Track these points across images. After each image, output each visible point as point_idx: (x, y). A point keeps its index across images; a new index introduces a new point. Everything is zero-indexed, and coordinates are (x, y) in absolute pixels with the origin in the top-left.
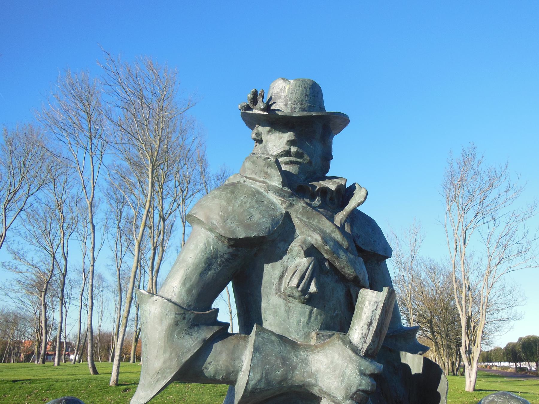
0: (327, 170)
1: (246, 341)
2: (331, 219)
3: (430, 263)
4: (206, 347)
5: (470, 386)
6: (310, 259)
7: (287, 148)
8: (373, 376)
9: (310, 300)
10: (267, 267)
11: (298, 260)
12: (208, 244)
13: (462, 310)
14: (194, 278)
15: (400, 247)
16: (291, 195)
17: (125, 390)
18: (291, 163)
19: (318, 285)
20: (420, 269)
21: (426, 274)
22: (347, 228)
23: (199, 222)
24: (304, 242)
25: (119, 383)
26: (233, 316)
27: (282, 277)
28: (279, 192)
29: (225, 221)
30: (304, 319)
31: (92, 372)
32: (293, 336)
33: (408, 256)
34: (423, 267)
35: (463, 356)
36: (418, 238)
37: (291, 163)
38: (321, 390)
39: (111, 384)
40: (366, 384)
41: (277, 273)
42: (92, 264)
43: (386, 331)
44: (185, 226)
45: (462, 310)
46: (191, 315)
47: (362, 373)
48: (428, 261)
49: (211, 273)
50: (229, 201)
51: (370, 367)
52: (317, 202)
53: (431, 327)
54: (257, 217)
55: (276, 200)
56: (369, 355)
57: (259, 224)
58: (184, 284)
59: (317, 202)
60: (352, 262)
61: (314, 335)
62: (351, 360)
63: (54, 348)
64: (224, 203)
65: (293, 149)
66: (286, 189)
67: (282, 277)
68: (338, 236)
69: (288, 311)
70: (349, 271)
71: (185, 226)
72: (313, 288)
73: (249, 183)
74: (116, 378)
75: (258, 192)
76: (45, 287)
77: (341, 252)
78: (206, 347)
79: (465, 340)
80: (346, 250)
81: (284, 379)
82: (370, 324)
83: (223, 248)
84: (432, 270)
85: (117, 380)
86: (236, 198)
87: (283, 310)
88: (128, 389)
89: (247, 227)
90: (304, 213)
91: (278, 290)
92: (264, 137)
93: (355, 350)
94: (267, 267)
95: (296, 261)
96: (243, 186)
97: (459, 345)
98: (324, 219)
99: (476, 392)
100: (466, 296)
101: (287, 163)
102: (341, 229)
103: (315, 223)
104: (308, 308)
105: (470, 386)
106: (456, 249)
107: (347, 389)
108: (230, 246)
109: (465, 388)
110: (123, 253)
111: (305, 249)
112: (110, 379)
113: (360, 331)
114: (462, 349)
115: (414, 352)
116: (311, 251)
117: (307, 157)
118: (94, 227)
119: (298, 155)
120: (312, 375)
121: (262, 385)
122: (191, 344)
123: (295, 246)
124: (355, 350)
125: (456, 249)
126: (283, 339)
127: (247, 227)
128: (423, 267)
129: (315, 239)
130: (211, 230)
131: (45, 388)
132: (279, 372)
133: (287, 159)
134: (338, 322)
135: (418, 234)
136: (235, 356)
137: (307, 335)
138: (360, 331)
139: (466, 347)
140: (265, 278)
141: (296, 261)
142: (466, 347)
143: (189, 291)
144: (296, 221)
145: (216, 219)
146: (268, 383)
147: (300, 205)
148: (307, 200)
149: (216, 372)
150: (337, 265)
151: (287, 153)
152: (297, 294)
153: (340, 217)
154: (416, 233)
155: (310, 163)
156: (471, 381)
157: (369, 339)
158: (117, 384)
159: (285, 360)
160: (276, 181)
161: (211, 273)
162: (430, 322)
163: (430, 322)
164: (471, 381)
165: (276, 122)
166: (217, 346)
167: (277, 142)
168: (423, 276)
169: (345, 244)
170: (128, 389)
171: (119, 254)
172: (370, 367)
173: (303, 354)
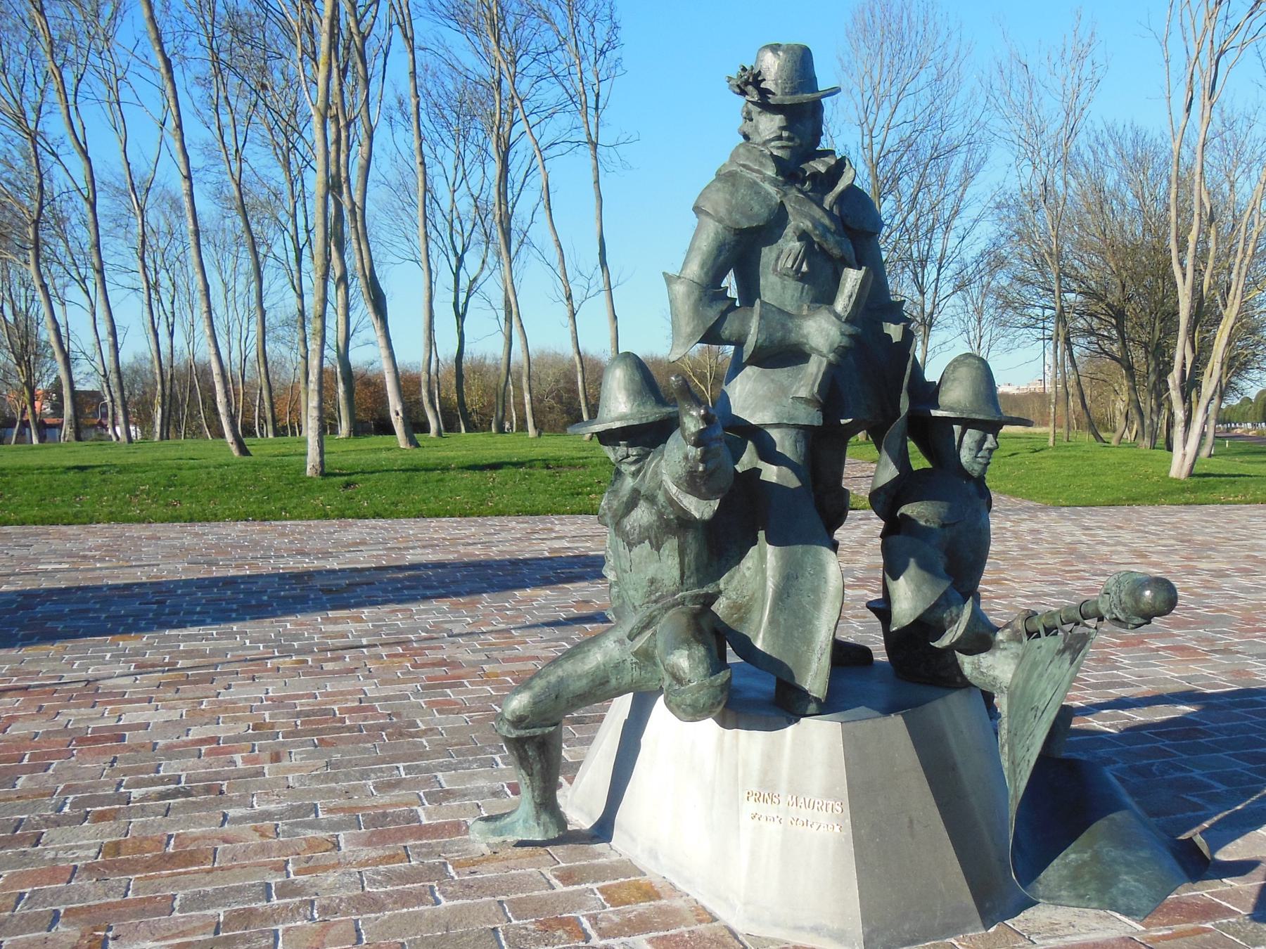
0: (818, 142)
1: (752, 311)
2: (820, 205)
3: (1135, 143)
4: (723, 316)
5: (1182, 467)
6: (803, 243)
7: (779, 133)
8: (850, 336)
9: (802, 278)
10: (765, 250)
11: (791, 244)
12: (717, 233)
13: (1184, 275)
14: (710, 263)
15: (1036, 100)
16: (785, 184)
17: (347, 485)
18: (783, 147)
19: (809, 265)
20: (1102, 159)
21: (1120, 175)
22: (836, 211)
23: (708, 214)
24: (797, 228)
25: (326, 470)
26: (576, 306)
27: (778, 258)
28: (774, 182)
29: (730, 213)
30: (797, 294)
31: (236, 453)
32: (788, 309)
33: (1057, 125)
34: (1111, 153)
35: (1175, 394)
36: (1086, 72)
37: (783, 147)
38: (811, 348)
39: (309, 473)
40: (845, 342)
41: (774, 255)
42: (185, 173)
43: (864, 301)
44: (412, 51)
45: (1184, 275)
46: (710, 292)
47: (842, 334)
48: (1130, 135)
49: (722, 258)
50: (732, 194)
51: (849, 329)
52: (807, 186)
53: (1119, 327)
54: (756, 208)
55: (772, 190)
56: (850, 320)
57: (760, 213)
58: (702, 266)
59: (807, 186)
60: (839, 244)
61: (805, 307)
62: (834, 324)
63: (58, 408)
64: (728, 196)
65: (785, 134)
66: (780, 178)
67: (778, 258)
68: (826, 221)
69: (784, 288)
70: (836, 252)
71: (412, 51)
72: (805, 268)
73: (746, 173)
74: (318, 459)
75: (755, 183)
76: (31, 237)
77: (829, 236)
78: (723, 316)
79: (1182, 352)
80: (833, 234)
81: (783, 339)
82: (851, 296)
83: (730, 237)
84: (1138, 163)
85: (322, 463)
86: (737, 191)
87: (779, 287)
88: (354, 483)
89: (749, 218)
90: (798, 200)
91: (775, 270)
92: (754, 115)
93: (838, 316)
94: (765, 250)
95: (790, 245)
96: (742, 177)
97: (1164, 369)
98: (815, 207)
99: (1196, 479)
100: (1202, 242)
101: (778, 148)
102: (829, 213)
103: (806, 209)
104: (800, 285)
105: (1182, 467)
106: (1188, 110)
107: (831, 346)
108: (735, 234)
109: (1168, 472)
110: (241, 139)
111: (868, 505)
112: (306, 464)
113: (842, 304)
114: (1174, 379)
115: (896, 323)
116: (803, 236)
117: (798, 141)
118: (168, 63)
119: (789, 139)
120: (805, 336)
121: (767, 343)
122: (712, 314)
123: (789, 231)
124: (838, 316)
125: (1188, 110)
126: (781, 311)
127: (749, 218)
128: (1111, 153)
129: (807, 224)
130: (720, 221)
131: (163, 482)
132: (779, 334)
133: (778, 143)
134: (824, 296)
135: (1088, 62)
136: (745, 322)
137: (800, 307)
138: (842, 304)
139: (1183, 372)
140: (763, 260)
141: (790, 245)
142: (1183, 372)
143: (706, 274)
144: (789, 209)
145: (723, 212)
146: (772, 342)
147: (793, 193)
148: (798, 186)
149: (731, 335)
150: (825, 246)
151: (780, 138)
152: (791, 273)
153: (829, 199)
154: (1081, 57)
155: (801, 145)
156: (1184, 455)
157: (849, 309)
158: (324, 474)
159: (783, 326)
160: (771, 171)
161: (722, 258)
162: (1120, 315)
163: (1120, 315)
164: (1184, 455)
165: (765, 104)
166: (730, 316)
167: (769, 125)
168: (1111, 179)
169: (833, 228)
170: (354, 483)
171: (229, 138)
172: (849, 329)
173: (797, 321)
